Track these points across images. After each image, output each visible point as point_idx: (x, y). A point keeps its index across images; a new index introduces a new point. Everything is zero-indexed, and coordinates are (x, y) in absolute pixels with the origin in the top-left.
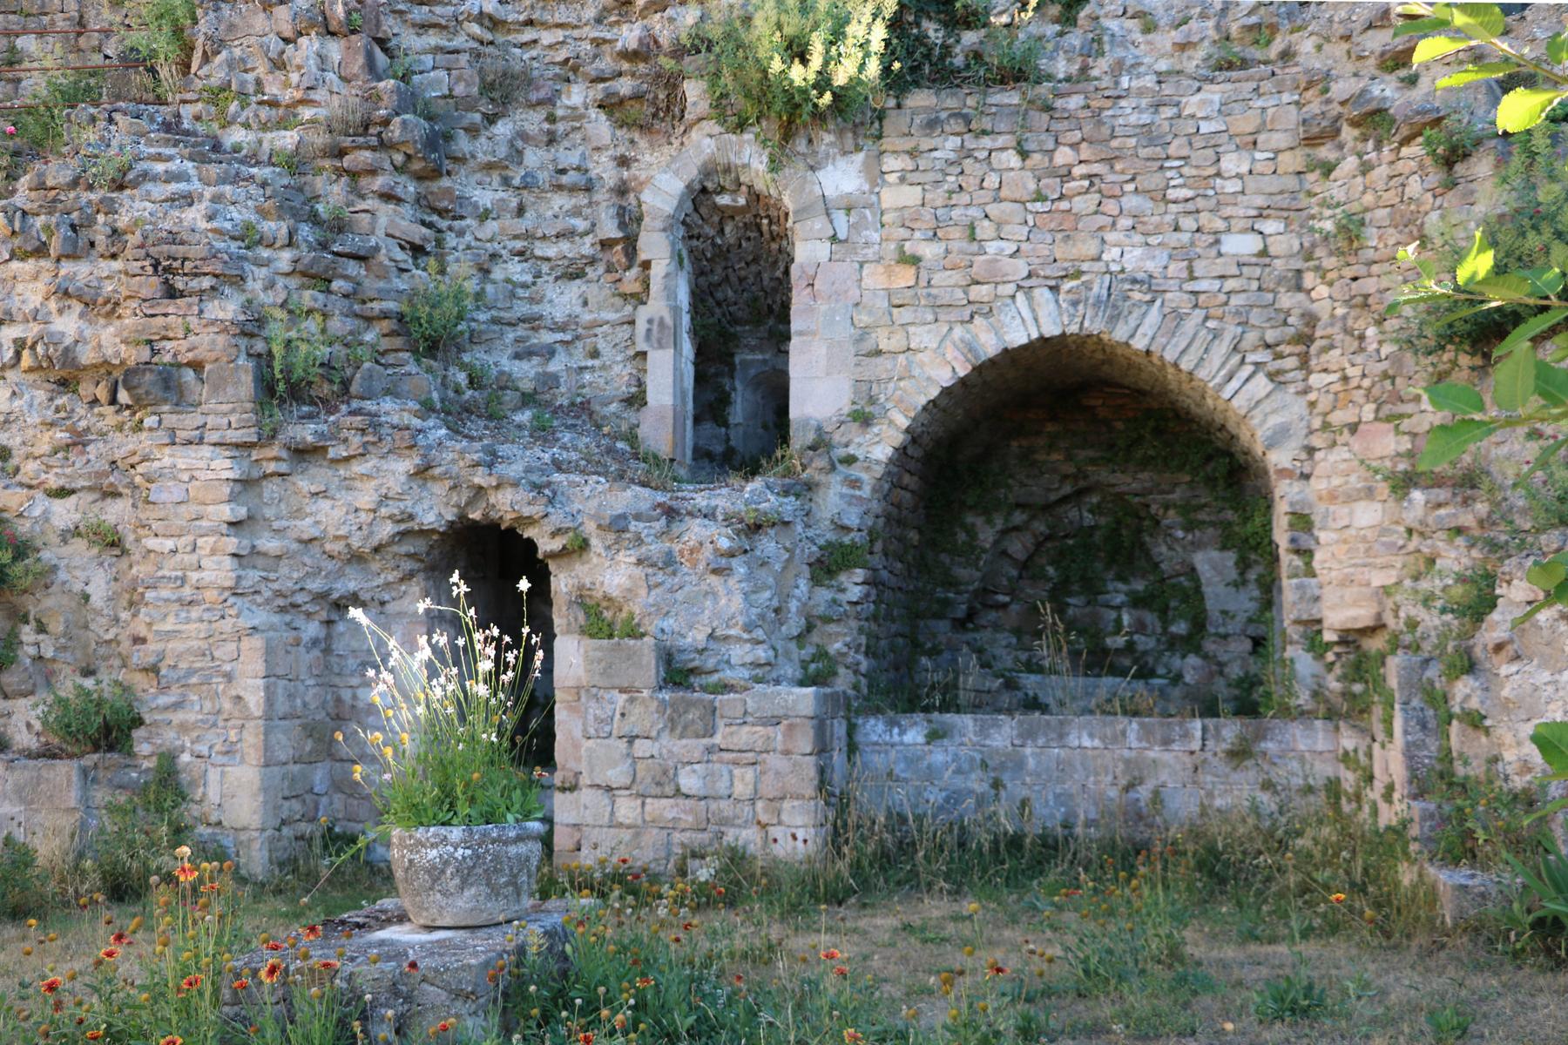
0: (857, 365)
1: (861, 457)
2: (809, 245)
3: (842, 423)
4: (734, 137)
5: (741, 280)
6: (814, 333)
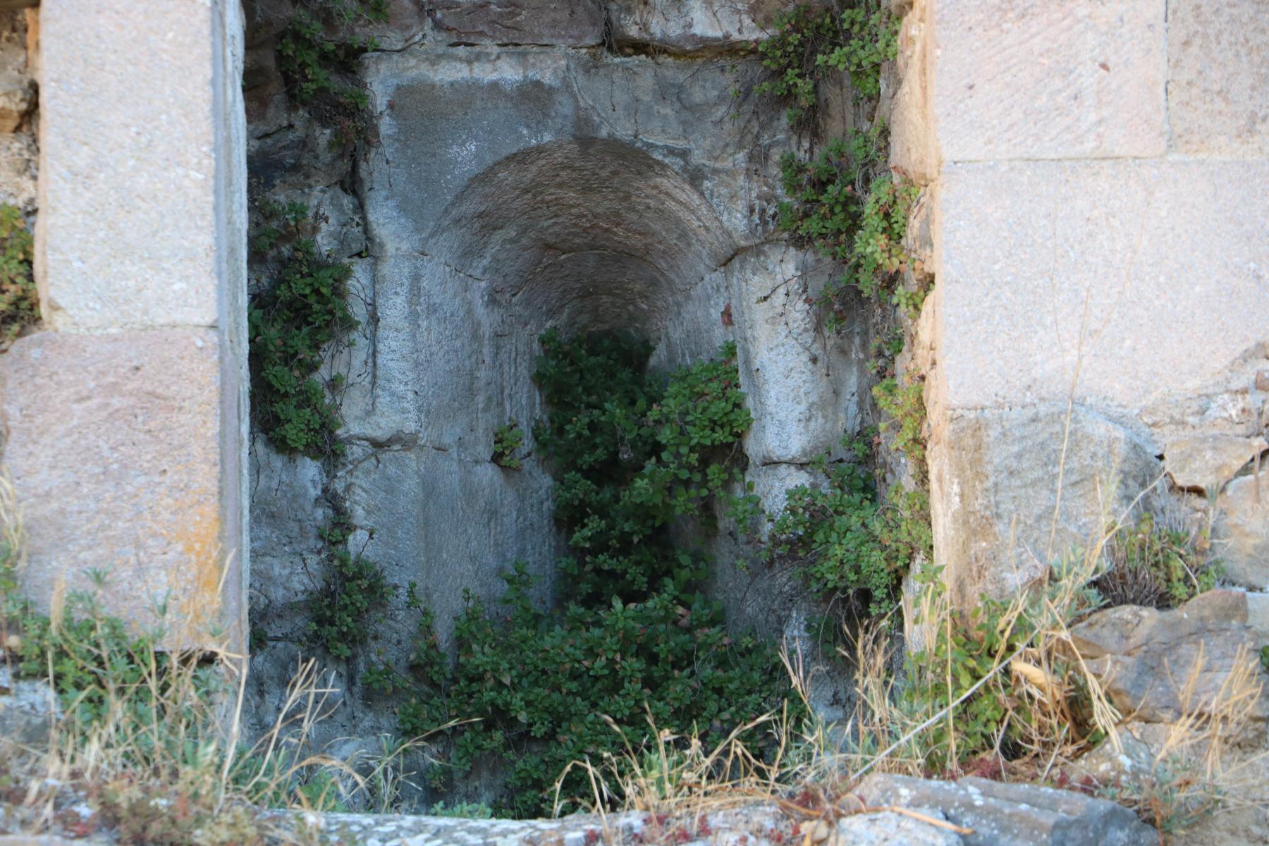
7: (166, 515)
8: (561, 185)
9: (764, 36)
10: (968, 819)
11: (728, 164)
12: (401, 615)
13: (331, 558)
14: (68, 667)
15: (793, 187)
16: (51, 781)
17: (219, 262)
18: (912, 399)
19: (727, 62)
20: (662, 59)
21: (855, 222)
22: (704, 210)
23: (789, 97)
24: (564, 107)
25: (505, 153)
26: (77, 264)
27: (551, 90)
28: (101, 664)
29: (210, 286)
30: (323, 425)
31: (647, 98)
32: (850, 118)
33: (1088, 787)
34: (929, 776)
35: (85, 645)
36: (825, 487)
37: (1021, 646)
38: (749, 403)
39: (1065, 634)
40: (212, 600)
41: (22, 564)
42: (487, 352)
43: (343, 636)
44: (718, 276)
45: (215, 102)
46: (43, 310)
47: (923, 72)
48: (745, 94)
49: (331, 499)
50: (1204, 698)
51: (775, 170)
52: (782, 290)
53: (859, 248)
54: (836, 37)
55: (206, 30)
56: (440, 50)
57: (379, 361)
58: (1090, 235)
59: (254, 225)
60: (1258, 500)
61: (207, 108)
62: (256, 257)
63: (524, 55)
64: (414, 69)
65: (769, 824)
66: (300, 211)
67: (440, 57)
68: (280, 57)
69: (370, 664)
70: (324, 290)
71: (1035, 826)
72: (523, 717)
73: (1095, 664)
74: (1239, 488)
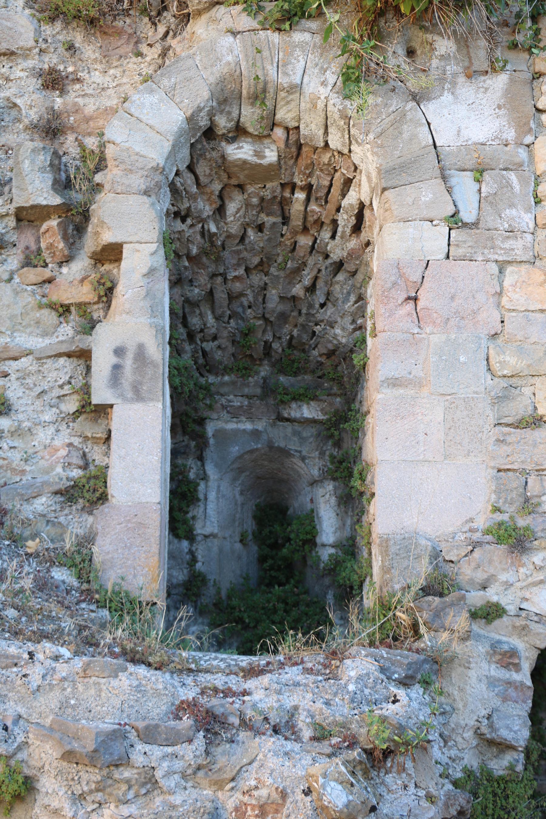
0: (500, 441)
1: (511, 609)
2: (411, 230)
3: (476, 545)
4: (275, 37)
5: (232, 297)
6: (418, 384)
7: (143, 560)
8: (263, 460)
9: (325, 418)
10: (382, 661)
11: (313, 455)
12: (211, 588)
13: (191, 570)
14: (113, 605)
15: (332, 463)
16: (107, 640)
17: (161, 484)
18: (367, 530)
19: (313, 425)
20: (294, 423)
21: (351, 475)
22: (306, 469)
23: (332, 436)
24: (265, 437)
25: (247, 450)
26: (120, 484)
27: (261, 432)
28: (122, 604)
29: (158, 491)
30: (190, 530)
31: (289, 435)
32: (350, 443)
33: (418, 651)
34: (370, 647)
35: (118, 599)
36: (340, 553)
37: (399, 607)
38: (318, 527)
39: (412, 605)
40: (156, 586)
41: (100, 573)
42: (239, 509)
43: (194, 594)
44: (309, 489)
45: (162, 437)
46: (109, 497)
47: (373, 433)
48: (319, 434)
49: (191, 553)
50: (453, 625)
51: (327, 458)
52: (328, 494)
53: (352, 483)
54: (346, 420)
55: (161, 415)
56: (229, 419)
57: (207, 511)
58: (421, 484)
59: (172, 470)
60: (469, 565)
61: (160, 438)
62: (172, 479)
63: (253, 421)
64: (220, 425)
65: (322, 661)
66: (185, 466)
67: (228, 421)
68: (181, 421)
69: (201, 603)
70: (192, 490)
71: (402, 664)
72: (247, 621)
73: (421, 614)
74: (464, 561)
